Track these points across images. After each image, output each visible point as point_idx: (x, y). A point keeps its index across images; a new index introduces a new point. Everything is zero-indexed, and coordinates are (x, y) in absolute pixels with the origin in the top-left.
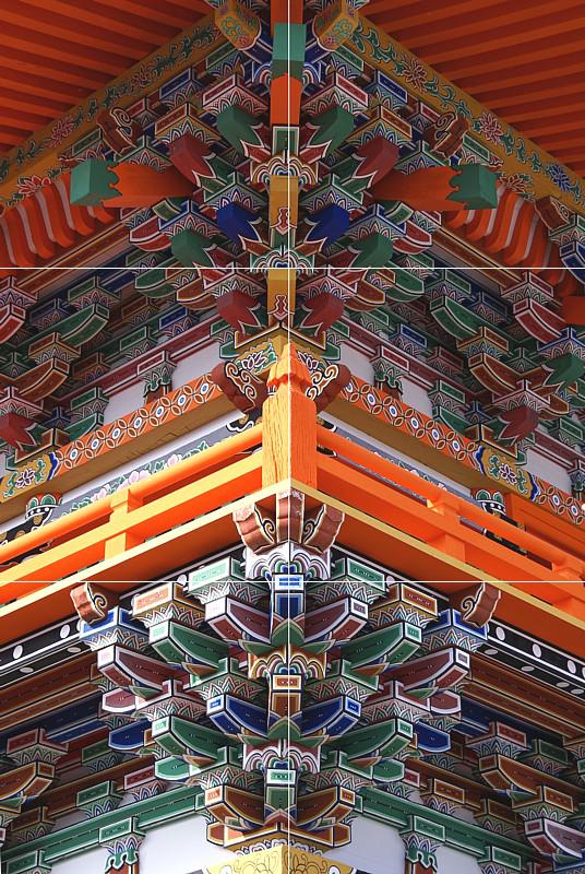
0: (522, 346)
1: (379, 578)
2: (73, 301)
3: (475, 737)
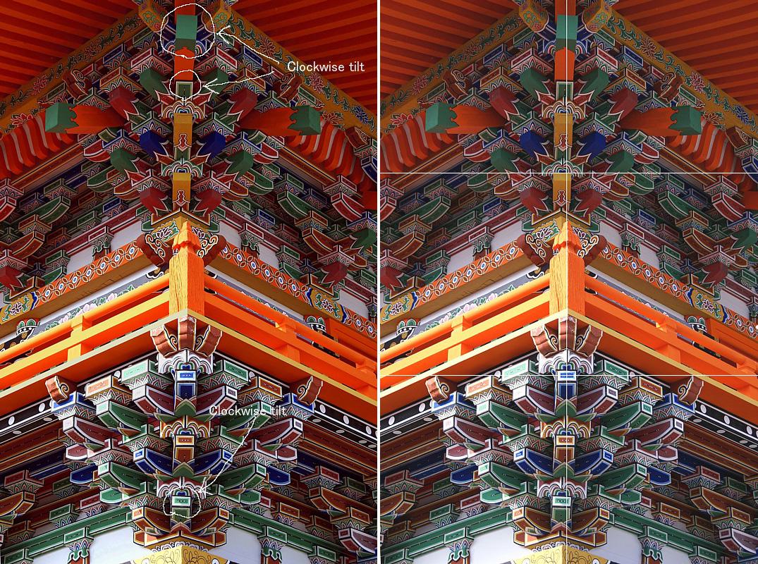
0: (336, 223)
1: (625, 373)
2: (427, 194)
3: (306, 475)
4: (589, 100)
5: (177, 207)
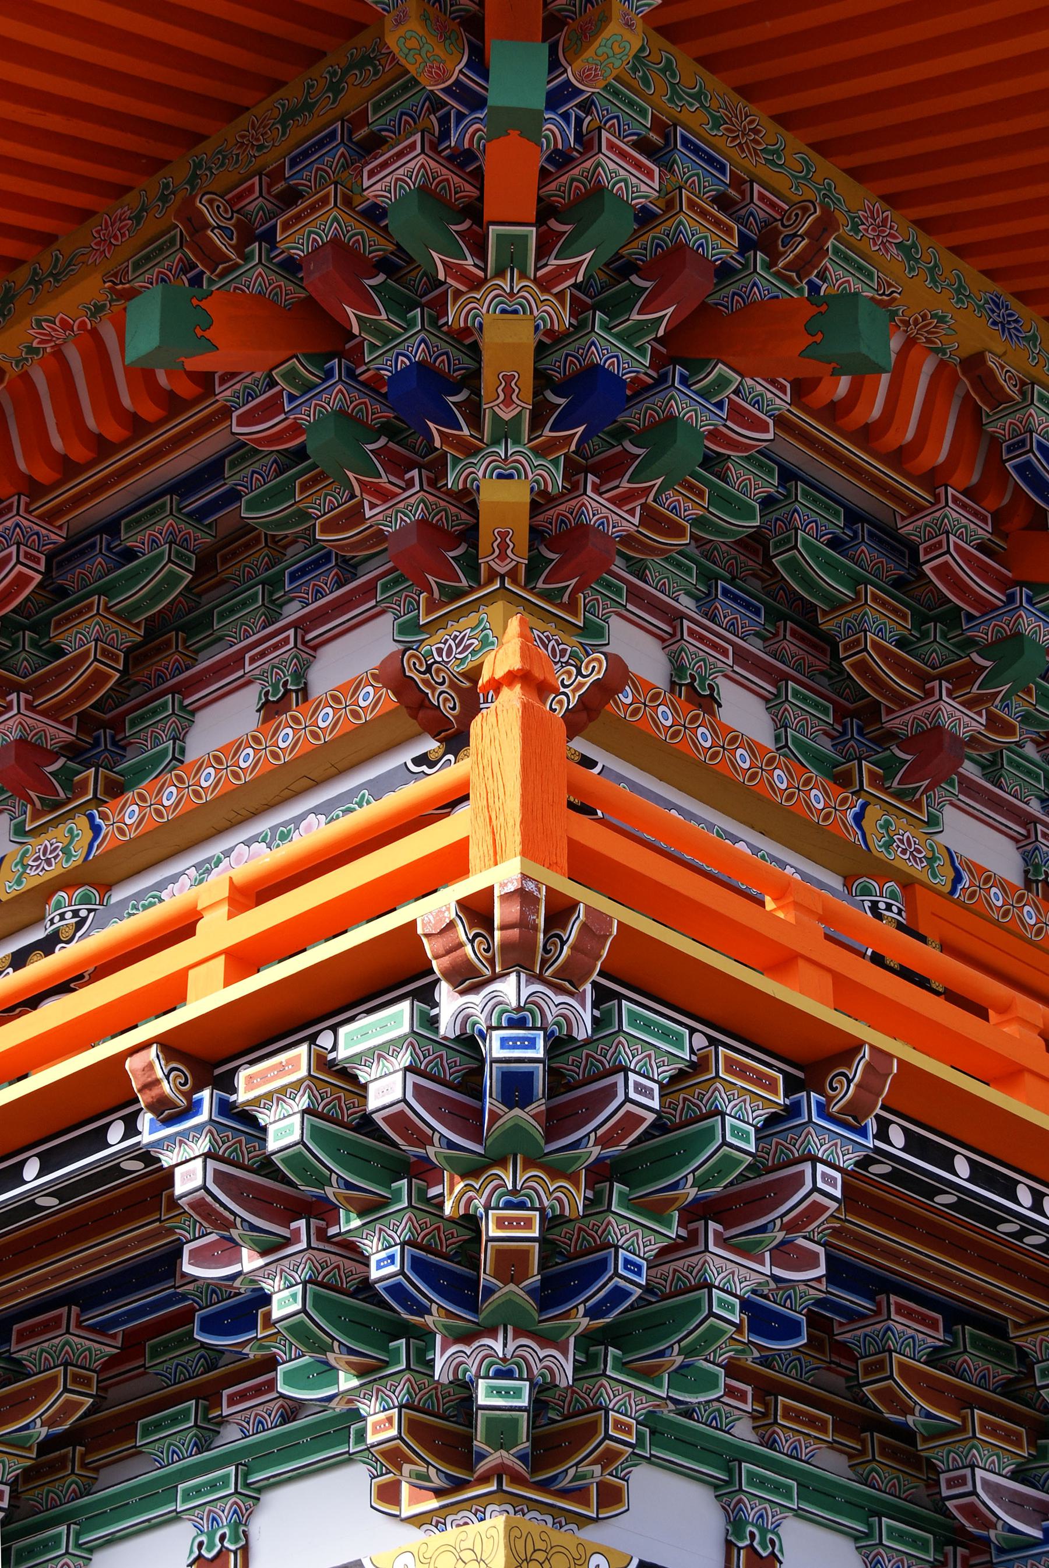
0: (936, 620)
3: (852, 1321)
4: (580, 279)
5: (493, 575)
